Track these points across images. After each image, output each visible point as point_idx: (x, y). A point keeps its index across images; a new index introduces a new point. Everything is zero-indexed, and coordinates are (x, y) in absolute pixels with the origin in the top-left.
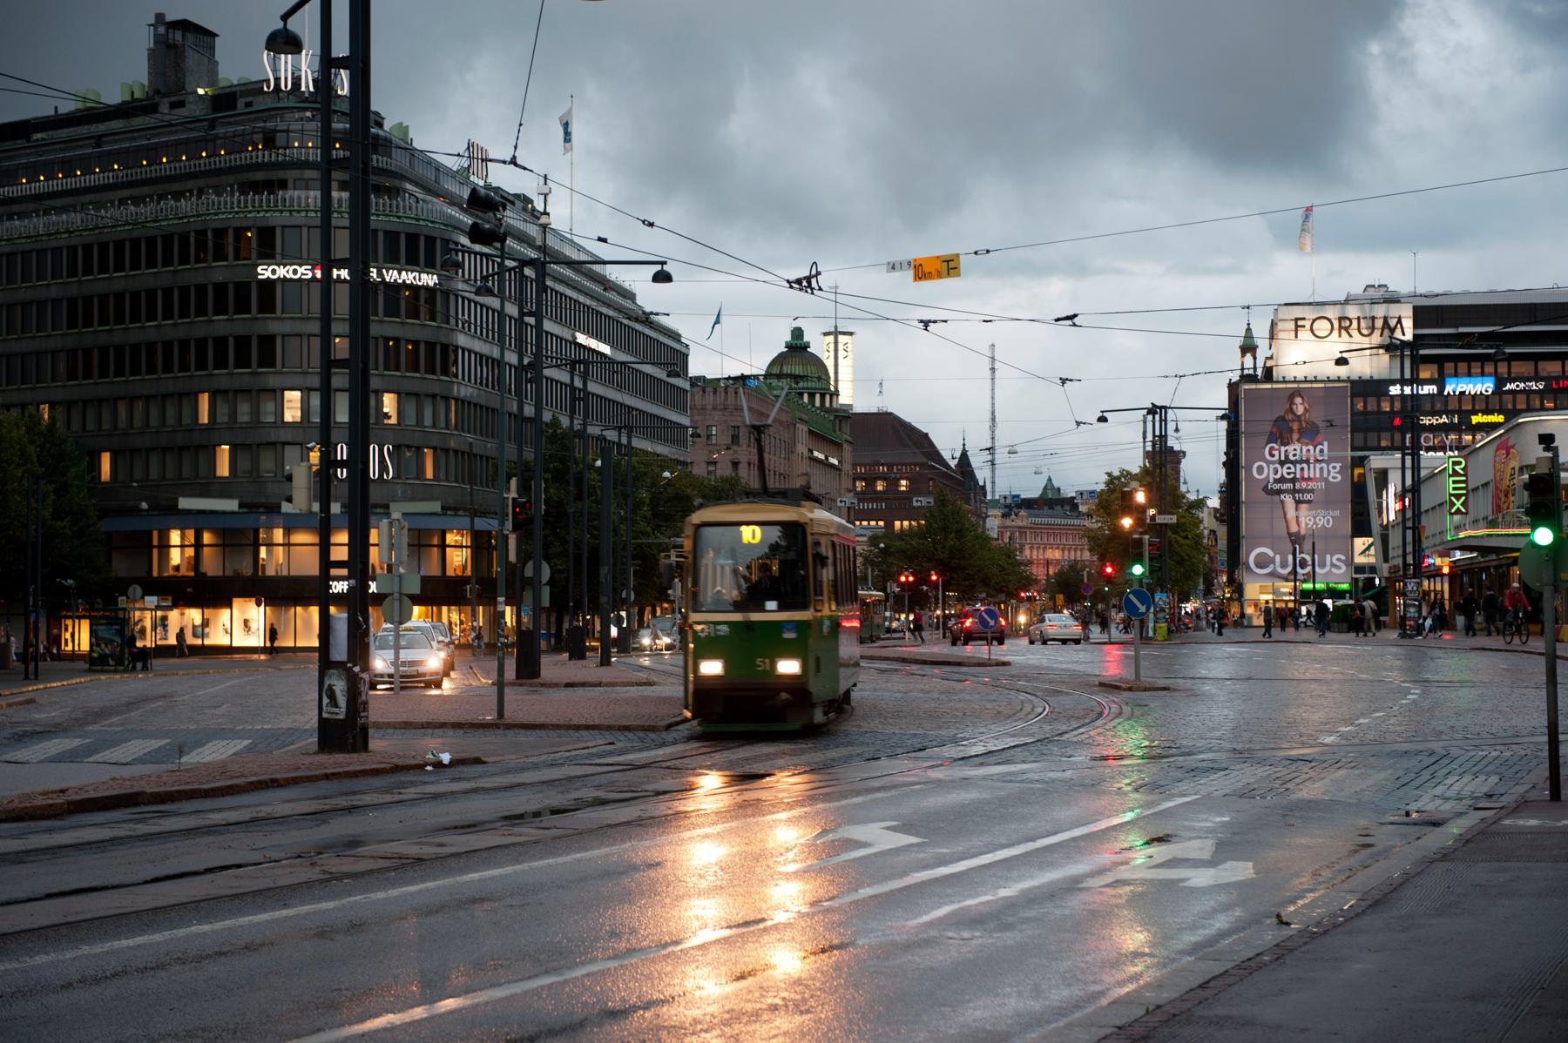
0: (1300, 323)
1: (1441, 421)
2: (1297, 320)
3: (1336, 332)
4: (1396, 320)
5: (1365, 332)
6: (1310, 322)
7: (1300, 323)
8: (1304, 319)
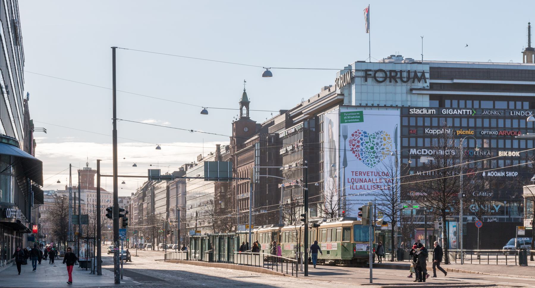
0: (357, 173)
3: (388, 80)
4: (421, 74)
5: (405, 80)
6: (374, 72)
7: (357, 173)
8: (370, 70)
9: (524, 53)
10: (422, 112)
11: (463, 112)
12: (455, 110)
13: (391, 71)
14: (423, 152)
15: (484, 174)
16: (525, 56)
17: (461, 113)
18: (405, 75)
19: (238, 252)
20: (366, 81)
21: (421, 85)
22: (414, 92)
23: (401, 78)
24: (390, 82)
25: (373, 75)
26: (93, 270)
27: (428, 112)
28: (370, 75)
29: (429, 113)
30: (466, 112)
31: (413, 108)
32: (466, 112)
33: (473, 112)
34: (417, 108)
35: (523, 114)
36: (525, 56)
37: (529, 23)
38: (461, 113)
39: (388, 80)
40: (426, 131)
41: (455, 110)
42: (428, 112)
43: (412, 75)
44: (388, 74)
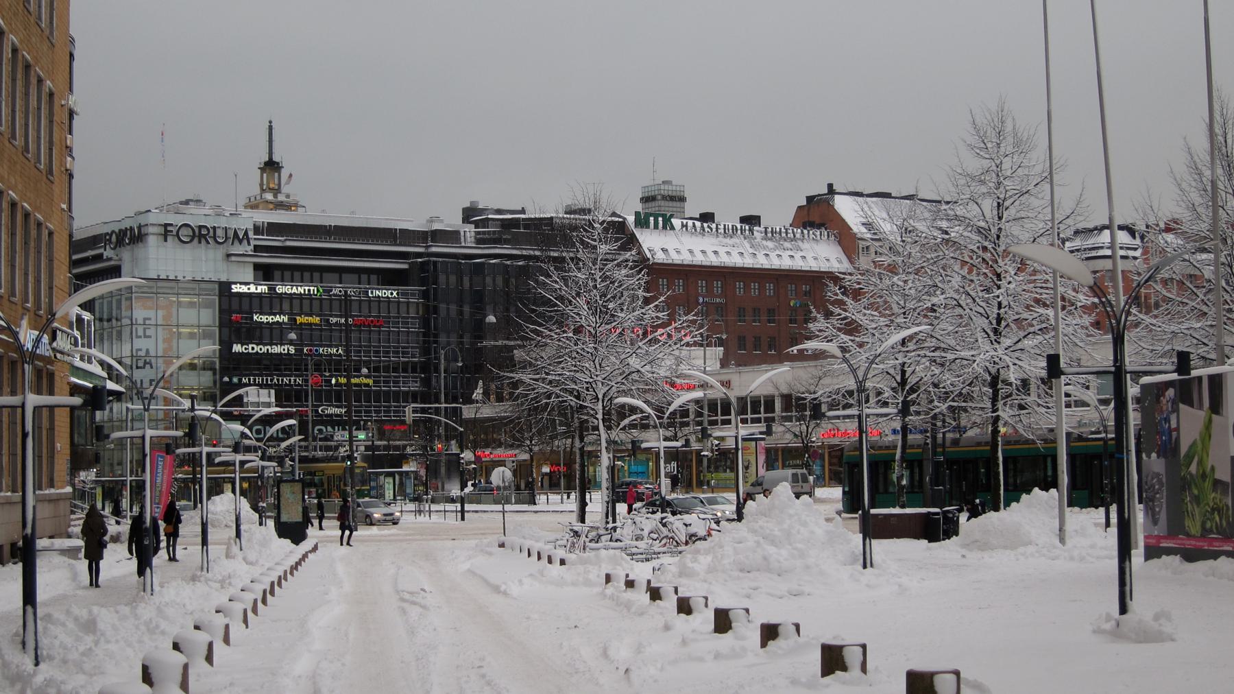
1: (275, 320)
2: (166, 225)
3: (196, 240)
8: (171, 225)
9: (262, 170)
10: (249, 289)
11: (305, 290)
12: (295, 288)
13: (200, 227)
14: (250, 349)
15: (333, 381)
16: (265, 175)
17: (303, 292)
18: (220, 233)
19: (662, 454)
20: (166, 240)
21: (238, 249)
22: (233, 258)
23: (214, 237)
24: (200, 242)
25: (174, 233)
26: (864, 435)
27: (256, 289)
28: (172, 231)
29: (259, 291)
30: (309, 290)
31: (235, 283)
32: (309, 290)
33: (318, 291)
34: (241, 283)
35: (385, 294)
36: (265, 175)
37: (270, 122)
38: (303, 292)
39: (196, 240)
40: (255, 318)
41: (295, 288)
42: (256, 289)
43: (231, 234)
44: (197, 230)
